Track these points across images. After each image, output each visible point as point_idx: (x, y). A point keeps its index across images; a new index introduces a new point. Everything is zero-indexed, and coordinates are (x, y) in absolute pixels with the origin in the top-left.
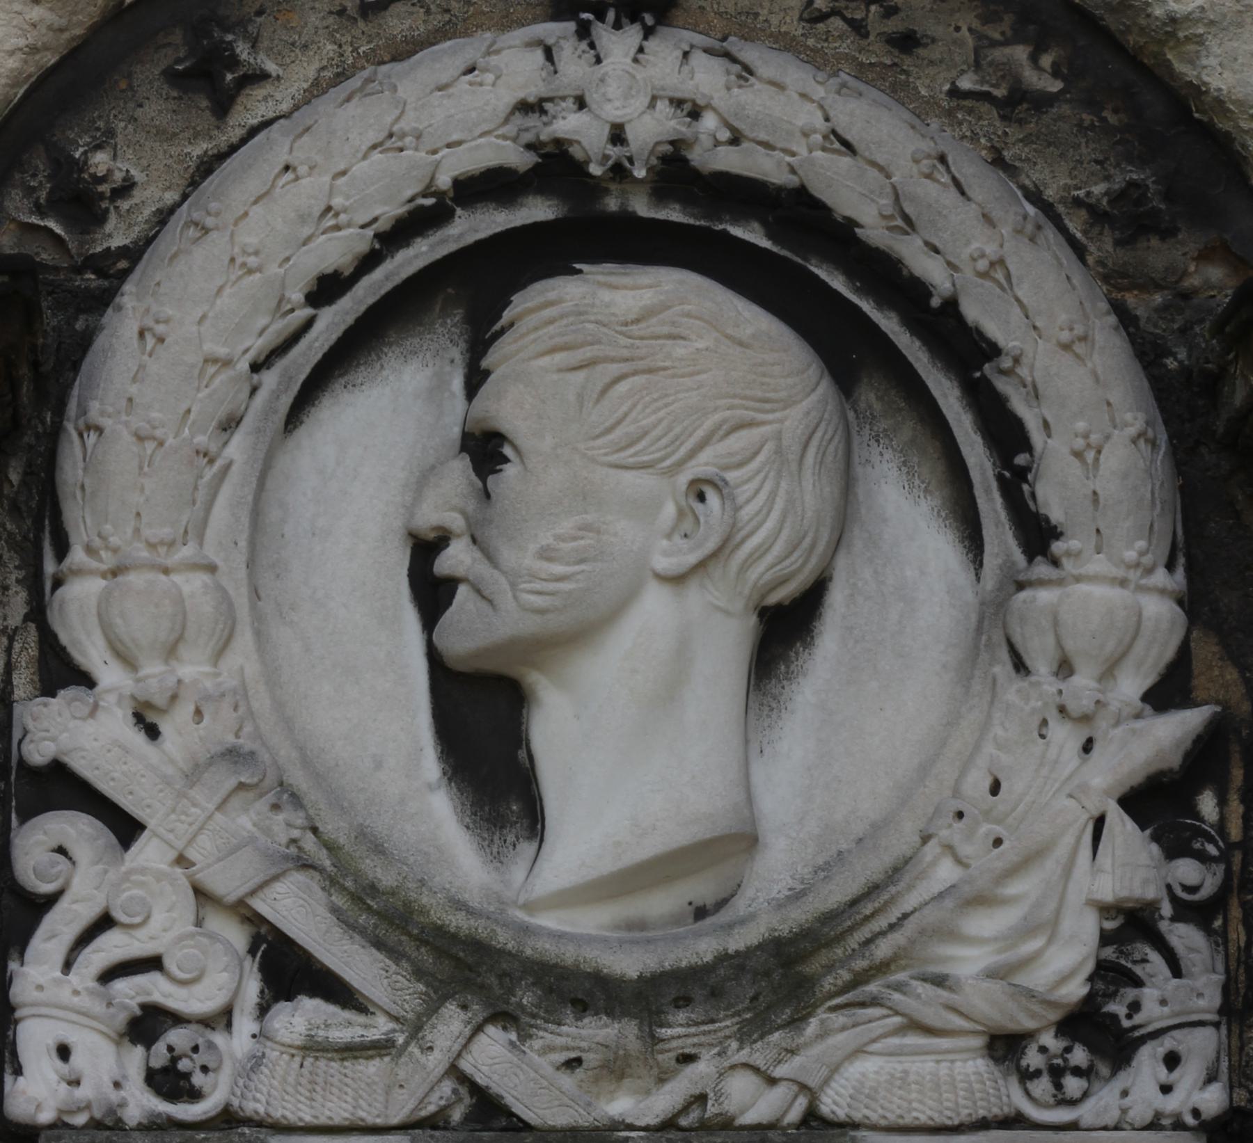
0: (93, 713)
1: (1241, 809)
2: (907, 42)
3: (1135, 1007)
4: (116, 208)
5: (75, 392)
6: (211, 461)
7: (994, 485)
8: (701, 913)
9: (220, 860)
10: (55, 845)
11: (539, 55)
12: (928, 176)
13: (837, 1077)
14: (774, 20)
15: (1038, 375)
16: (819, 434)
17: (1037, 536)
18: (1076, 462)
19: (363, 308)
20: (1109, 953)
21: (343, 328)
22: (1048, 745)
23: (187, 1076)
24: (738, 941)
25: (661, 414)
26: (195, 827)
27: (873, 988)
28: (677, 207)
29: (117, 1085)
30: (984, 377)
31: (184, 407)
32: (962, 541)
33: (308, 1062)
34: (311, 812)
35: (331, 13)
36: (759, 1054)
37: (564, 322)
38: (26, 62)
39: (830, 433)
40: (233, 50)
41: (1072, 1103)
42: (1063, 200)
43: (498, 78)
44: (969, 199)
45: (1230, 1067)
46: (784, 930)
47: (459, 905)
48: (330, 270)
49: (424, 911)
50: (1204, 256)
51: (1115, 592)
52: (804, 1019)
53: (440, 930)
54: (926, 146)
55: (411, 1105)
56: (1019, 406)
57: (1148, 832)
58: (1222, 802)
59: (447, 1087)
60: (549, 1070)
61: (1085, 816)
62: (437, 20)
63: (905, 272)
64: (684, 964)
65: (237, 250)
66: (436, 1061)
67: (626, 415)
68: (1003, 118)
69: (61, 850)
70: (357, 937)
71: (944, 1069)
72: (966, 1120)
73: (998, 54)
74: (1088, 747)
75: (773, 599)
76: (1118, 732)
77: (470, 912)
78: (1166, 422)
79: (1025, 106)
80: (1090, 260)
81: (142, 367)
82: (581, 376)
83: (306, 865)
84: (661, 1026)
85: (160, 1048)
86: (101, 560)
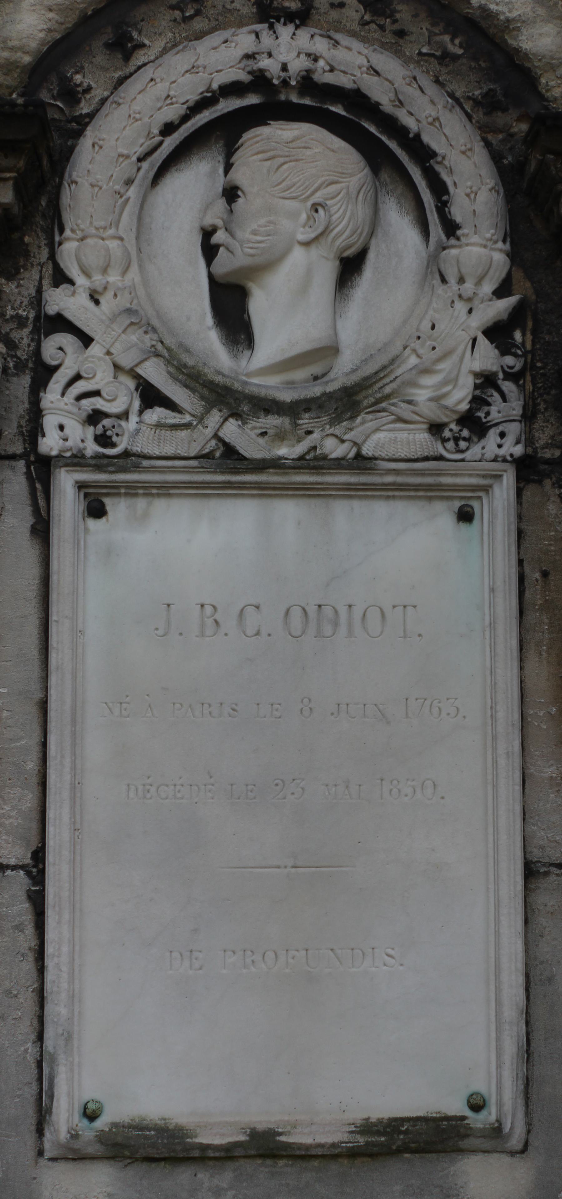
0: (74, 293)
1: (531, 337)
2: (401, 34)
3: (488, 414)
4: (85, 98)
5: (68, 169)
6: (121, 197)
7: (434, 209)
8: (316, 378)
9: (124, 352)
10: (58, 346)
11: (253, 36)
12: (409, 85)
13: (368, 440)
14: (348, 25)
15: (452, 163)
16: (364, 188)
17: (451, 228)
18: (467, 198)
19: (183, 138)
20: (478, 392)
21: (174, 145)
22: (454, 310)
23: (110, 437)
24: (330, 388)
25: (301, 176)
26: (114, 340)
27: (383, 405)
28: (309, 98)
29: (83, 441)
30: (430, 165)
31: (110, 174)
32: (421, 233)
33: (158, 431)
34: (161, 335)
35: (171, 21)
36: (338, 430)
37: (263, 142)
38: (47, 35)
39: (369, 188)
40: (131, 34)
41: (462, 451)
42: (463, 97)
43: (237, 45)
44: (425, 94)
45: (525, 438)
46: (348, 384)
47: (219, 373)
48: (169, 121)
49: (205, 375)
50: (519, 120)
51: (482, 250)
52: (356, 417)
53: (212, 382)
54: (408, 73)
55: (199, 448)
56: (445, 176)
57: (494, 345)
58: (524, 335)
59: (213, 443)
60: (254, 436)
61: (469, 338)
62: (213, 23)
63: (399, 123)
64: (309, 397)
65: (131, 112)
66: (209, 432)
67: (287, 177)
68: (439, 64)
69: (61, 349)
70: (178, 383)
71: (411, 437)
72: (420, 457)
73: (438, 38)
74: (470, 311)
75: (346, 254)
76: (482, 306)
77: (224, 376)
78: (503, 185)
79: (448, 59)
80: (474, 121)
81: (93, 158)
82: (268, 163)
83: (158, 355)
84: (299, 419)
85: (100, 427)
86: (77, 235)
